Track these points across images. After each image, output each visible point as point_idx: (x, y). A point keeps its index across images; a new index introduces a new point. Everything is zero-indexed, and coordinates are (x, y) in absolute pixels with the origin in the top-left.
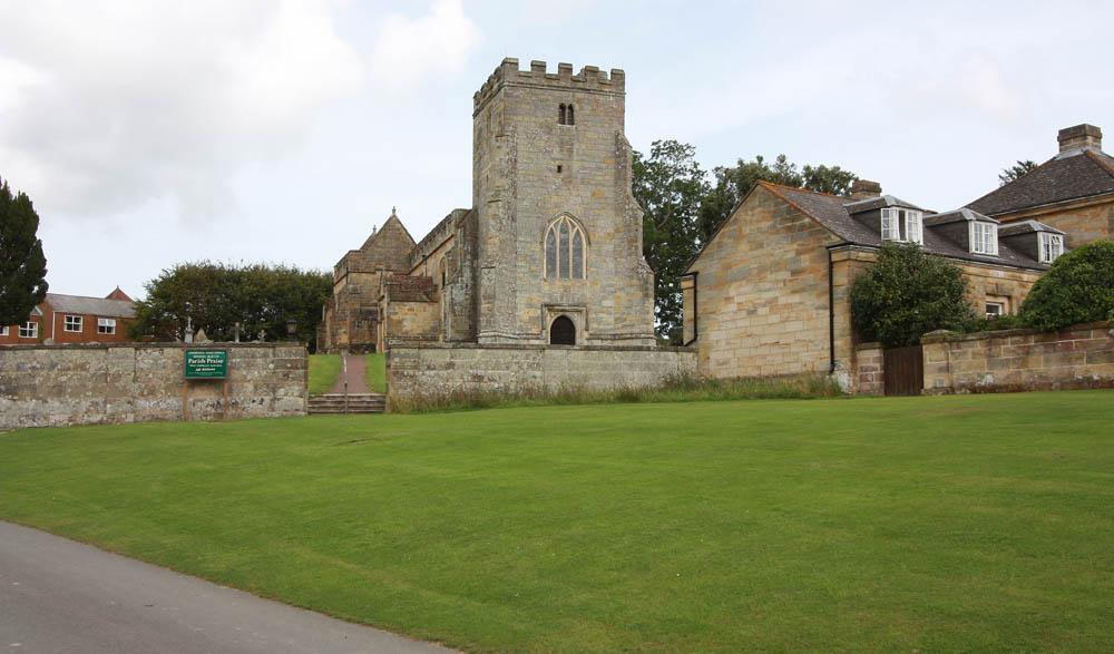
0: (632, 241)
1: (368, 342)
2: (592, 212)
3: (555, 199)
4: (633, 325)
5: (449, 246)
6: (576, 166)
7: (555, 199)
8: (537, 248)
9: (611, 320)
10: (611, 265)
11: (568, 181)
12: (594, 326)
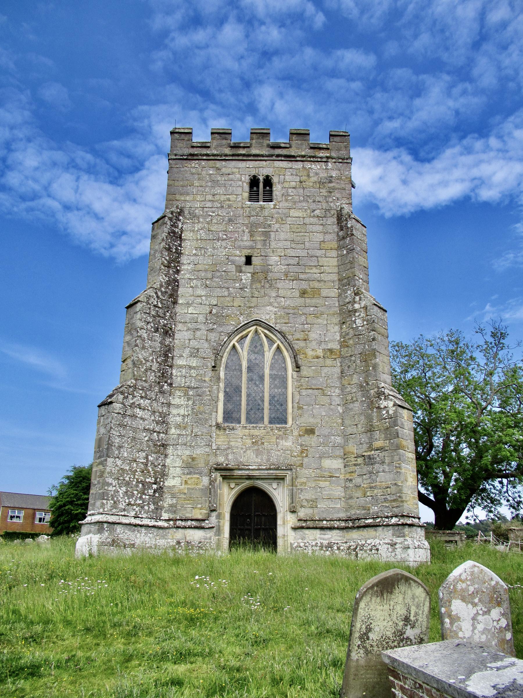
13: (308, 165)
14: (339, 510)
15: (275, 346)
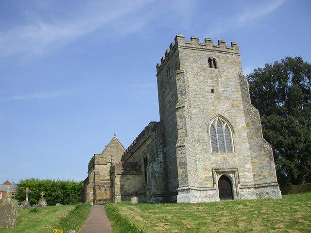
0: (257, 130)
1: (105, 198)
2: (233, 115)
3: (212, 107)
4: (266, 178)
5: (148, 143)
6: (221, 89)
7: (212, 107)
8: (206, 135)
9: (251, 176)
10: (247, 144)
11: (218, 98)
12: (242, 180)
13: (227, 55)
14: (251, 182)
15: (225, 124)
